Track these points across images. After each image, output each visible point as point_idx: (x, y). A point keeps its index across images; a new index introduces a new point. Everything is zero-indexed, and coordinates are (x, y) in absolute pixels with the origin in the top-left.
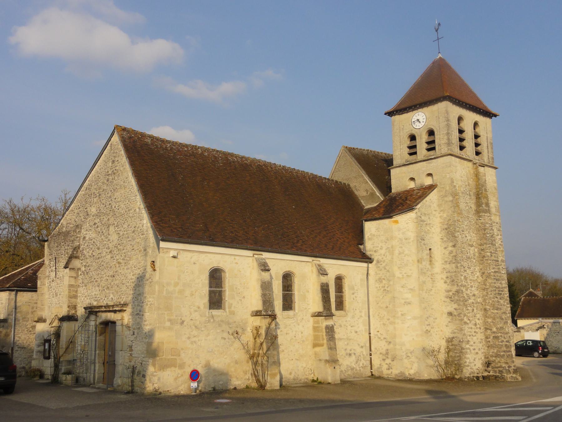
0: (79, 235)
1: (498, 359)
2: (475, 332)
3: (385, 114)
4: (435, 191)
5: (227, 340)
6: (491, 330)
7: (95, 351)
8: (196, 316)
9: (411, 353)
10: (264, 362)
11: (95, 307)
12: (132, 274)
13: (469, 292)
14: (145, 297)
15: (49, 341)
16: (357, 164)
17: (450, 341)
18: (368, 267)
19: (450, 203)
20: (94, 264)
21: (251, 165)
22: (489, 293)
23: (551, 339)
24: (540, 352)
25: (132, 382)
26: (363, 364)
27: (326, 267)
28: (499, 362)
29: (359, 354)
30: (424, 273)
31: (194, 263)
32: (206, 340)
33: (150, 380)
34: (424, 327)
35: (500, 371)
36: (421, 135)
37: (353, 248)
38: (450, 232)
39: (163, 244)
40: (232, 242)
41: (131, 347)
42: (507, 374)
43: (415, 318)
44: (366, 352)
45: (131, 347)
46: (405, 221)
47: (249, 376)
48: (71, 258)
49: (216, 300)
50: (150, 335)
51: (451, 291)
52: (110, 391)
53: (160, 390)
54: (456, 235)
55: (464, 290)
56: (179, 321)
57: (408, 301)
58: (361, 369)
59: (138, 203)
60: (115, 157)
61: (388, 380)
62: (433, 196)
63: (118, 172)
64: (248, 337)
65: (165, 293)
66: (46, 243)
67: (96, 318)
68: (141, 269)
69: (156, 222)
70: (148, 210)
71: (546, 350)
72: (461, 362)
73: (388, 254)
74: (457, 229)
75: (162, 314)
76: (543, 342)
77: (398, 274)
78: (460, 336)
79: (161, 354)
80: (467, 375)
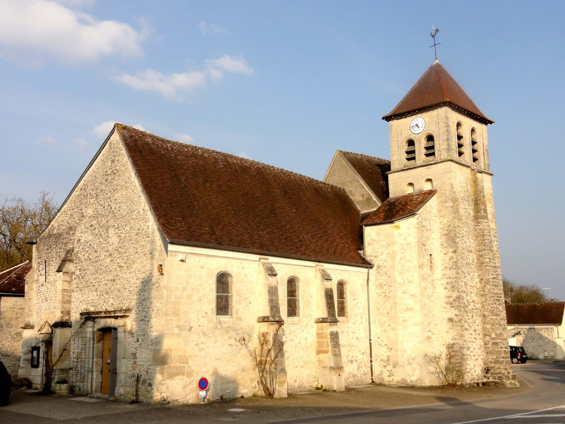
0: (73, 238)
1: (498, 365)
2: (475, 338)
3: (383, 119)
4: (435, 196)
5: (234, 347)
6: (490, 336)
7: (93, 359)
8: (204, 321)
9: (413, 359)
10: (272, 369)
11: (93, 313)
12: (135, 278)
13: (468, 298)
14: (151, 302)
15: (37, 349)
16: (353, 168)
17: (450, 347)
18: (368, 273)
19: (451, 209)
20: (91, 268)
21: (250, 168)
22: (488, 299)
23: (527, 345)
24: (519, 357)
25: (137, 391)
26: (364, 371)
27: (329, 272)
28: (499, 368)
29: (360, 361)
30: (426, 279)
31: (202, 267)
32: (213, 347)
33: (158, 389)
34: (425, 333)
35: (499, 377)
36: (420, 141)
37: (351, 251)
38: (451, 238)
39: (171, 247)
40: (239, 245)
41: (134, 354)
42: (507, 380)
43: (416, 324)
44: (367, 358)
45: (135, 355)
46: (405, 227)
47: (255, 383)
48: (64, 261)
49: (223, 306)
50: (158, 341)
51: (451, 297)
52: (112, 401)
53: (169, 400)
54: (457, 241)
55: (464, 296)
56: (188, 327)
57: (409, 307)
58: (362, 375)
59: (143, 205)
60: (115, 156)
61: (389, 386)
62: (433, 202)
63: (118, 172)
64: (254, 344)
65: (173, 297)
66: (34, 246)
67: (94, 324)
68: (146, 273)
69: (163, 224)
70: (155, 212)
71: (524, 356)
72: (463, 368)
73: (389, 259)
74: (458, 235)
75: (171, 320)
76: (522, 348)
77: (399, 279)
78: (461, 342)
79: (169, 362)
80: (468, 382)
